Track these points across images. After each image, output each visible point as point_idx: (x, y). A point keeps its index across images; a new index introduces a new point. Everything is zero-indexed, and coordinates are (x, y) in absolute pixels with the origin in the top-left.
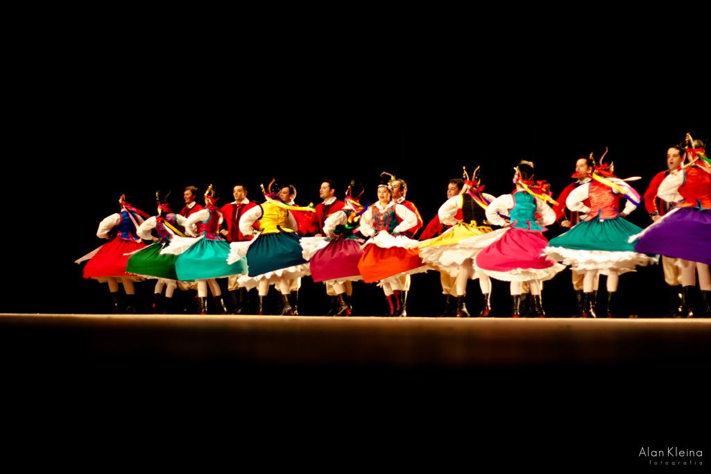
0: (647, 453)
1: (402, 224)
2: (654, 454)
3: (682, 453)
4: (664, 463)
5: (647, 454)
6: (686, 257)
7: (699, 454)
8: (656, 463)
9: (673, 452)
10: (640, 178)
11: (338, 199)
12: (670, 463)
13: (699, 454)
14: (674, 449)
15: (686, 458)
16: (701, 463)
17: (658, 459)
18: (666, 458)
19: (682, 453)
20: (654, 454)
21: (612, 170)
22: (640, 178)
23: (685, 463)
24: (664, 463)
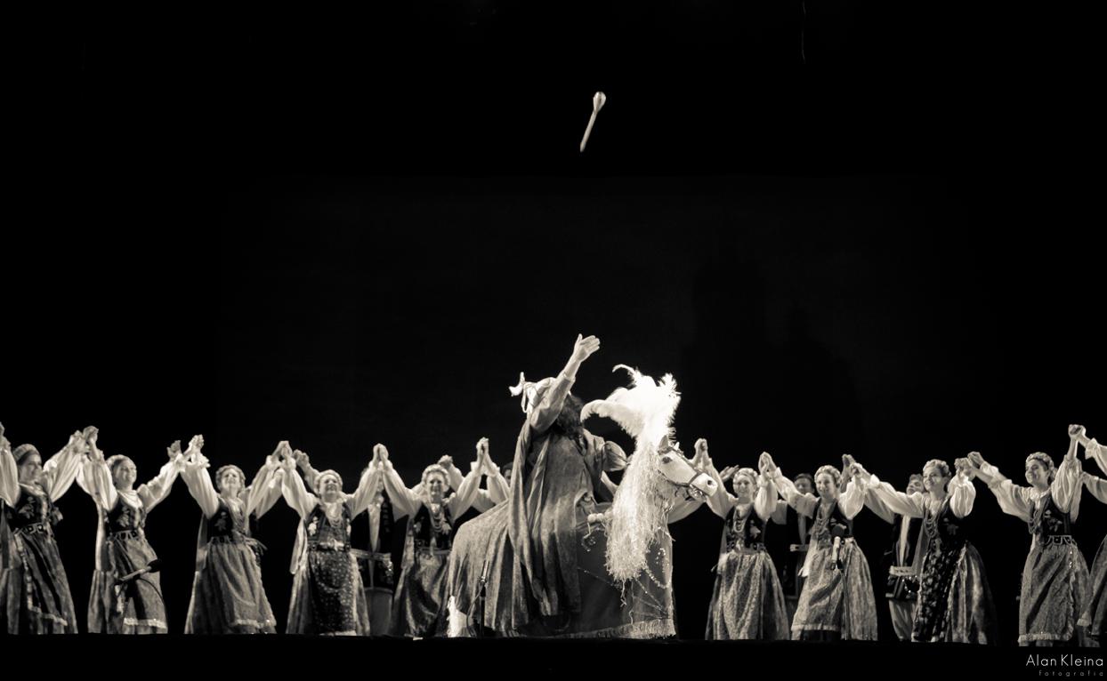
0: (1035, 662)
1: (371, 514)
2: (1045, 662)
3: (1078, 662)
4: (1097, 674)
5: (1035, 662)
6: (115, 645)
7: (1099, 662)
8: (1047, 674)
9: (1068, 660)
10: (522, 374)
11: (319, 517)
12: (1078, 674)
13: (1099, 662)
14: (1069, 657)
15: (1083, 668)
16: (1101, 674)
17: (1049, 668)
18: (1059, 667)
19: (1078, 662)
20: (1045, 662)
21: (197, 573)
22: (522, 374)
23: (1082, 674)
24: (1056, 673)
